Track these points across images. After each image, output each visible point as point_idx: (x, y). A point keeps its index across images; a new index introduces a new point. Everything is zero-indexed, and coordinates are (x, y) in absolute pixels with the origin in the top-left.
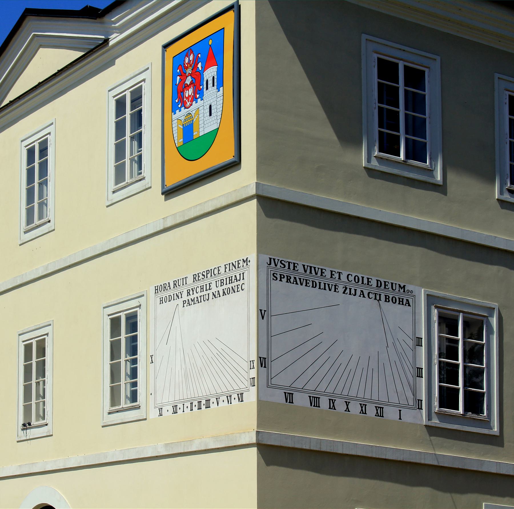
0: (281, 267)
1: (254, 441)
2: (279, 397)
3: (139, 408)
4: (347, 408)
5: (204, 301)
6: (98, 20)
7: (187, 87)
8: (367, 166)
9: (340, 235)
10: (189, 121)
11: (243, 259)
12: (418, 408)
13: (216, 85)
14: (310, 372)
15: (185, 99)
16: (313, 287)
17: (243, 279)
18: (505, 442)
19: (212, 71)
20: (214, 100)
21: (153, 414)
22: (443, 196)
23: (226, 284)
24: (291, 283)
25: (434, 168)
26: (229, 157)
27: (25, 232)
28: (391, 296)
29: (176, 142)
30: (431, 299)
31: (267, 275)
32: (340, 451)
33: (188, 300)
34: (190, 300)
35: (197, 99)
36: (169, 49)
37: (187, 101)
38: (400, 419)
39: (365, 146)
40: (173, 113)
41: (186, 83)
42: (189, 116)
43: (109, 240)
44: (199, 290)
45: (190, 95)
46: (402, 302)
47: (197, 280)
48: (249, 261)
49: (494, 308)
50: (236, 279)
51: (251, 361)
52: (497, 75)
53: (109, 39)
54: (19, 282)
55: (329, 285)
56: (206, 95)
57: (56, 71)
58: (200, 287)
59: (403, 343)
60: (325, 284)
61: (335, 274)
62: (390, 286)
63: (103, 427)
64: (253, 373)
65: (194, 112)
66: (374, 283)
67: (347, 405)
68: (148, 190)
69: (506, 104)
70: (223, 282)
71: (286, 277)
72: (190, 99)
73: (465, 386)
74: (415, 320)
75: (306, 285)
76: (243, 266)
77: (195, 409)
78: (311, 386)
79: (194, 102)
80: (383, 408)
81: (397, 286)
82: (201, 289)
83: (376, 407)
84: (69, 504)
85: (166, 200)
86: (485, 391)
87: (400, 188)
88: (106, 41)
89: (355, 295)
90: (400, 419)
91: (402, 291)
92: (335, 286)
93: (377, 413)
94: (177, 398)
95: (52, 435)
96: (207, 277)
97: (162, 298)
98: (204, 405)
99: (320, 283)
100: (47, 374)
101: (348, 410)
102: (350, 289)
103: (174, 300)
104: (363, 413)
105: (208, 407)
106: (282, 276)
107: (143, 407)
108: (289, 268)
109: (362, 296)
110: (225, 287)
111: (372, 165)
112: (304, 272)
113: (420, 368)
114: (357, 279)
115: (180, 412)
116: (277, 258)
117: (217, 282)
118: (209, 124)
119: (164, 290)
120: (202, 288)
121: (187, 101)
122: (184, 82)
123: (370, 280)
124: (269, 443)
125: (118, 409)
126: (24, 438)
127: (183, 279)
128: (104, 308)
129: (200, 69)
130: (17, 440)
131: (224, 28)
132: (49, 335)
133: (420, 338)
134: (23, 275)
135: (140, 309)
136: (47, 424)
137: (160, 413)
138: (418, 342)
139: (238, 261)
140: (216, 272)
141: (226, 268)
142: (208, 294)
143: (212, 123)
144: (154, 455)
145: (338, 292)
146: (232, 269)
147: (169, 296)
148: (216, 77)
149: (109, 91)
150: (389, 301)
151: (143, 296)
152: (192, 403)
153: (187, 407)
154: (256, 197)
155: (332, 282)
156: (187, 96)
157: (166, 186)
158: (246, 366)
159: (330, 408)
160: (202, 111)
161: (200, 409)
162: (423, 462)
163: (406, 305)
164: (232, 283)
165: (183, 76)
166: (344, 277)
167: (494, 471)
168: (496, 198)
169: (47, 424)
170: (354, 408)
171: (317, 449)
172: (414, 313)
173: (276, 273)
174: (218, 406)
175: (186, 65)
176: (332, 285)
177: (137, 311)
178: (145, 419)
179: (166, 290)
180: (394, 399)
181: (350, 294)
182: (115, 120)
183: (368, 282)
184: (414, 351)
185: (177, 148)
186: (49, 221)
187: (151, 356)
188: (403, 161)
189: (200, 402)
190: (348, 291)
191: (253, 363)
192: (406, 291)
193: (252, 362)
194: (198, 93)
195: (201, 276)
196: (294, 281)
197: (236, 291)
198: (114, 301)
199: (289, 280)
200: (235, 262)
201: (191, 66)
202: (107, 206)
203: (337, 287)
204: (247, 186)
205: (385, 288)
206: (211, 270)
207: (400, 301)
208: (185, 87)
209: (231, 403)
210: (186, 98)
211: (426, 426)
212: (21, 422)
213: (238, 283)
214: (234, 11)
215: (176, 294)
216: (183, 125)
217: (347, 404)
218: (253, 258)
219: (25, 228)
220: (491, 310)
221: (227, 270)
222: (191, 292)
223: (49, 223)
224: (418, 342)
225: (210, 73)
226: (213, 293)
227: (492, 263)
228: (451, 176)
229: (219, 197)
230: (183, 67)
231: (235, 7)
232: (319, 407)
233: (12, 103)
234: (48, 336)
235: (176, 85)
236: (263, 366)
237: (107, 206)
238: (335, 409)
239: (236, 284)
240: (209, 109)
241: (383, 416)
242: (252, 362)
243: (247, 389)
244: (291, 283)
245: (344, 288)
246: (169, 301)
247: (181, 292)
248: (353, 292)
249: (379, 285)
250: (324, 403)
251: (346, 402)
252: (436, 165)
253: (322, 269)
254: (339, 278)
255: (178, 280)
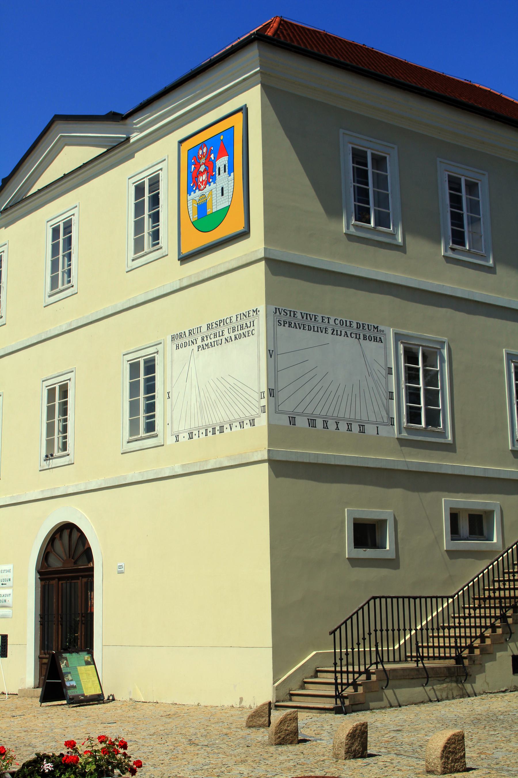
0: (284, 315)
1: (266, 457)
2: (284, 421)
3: (157, 436)
4: (337, 427)
5: (217, 345)
6: (121, 122)
7: (201, 173)
8: (347, 232)
9: (328, 288)
10: (203, 200)
11: (253, 310)
12: (391, 425)
13: (227, 171)
14: (308, 399)
15: (199, 183)
16: (308, 330)
17: (253, 326)
18: (457, 449)
19: (223, 160)
20: (226, 183)
21: (170, 440)
22: (403, 254)
23: (238, 330)
24: (292, 327)
25: (396, 233)
26: (240, 227)
27: (49, 296)
28: (368, 336)
29: (191, 218)
30: (398, 337)
31: (274, 321)
32: (333, 463)
33: (203, 345)
34: (204, 345)
35: (210, 182)
36: (184, 144)
37: (201, 185)
38: (378, 434)
39: (345, 217)
40: (188, 195)
41: (200, 170)
42: (203, 197)
43: (129, 300)
44: (212, 336)
45: (204, 179)
46: (376, 339)
47: (211, 328)
48: (259, 311)
49: (445, 342)
50: (247, 326)
51: (261, 392)
52: (439, 159)
53: (130, 137)
54: (43, 337)
55: (320, 328)
56: (219, 179)
57: (82, 164)
58: (213, 334)
59: (378, 373)
60: (318, 327)
61: (325, 319)
62: (366, 327)
63: (122, 454)
64: (264, 402)
65: (207, 193)
66: (354, 325)
67: (337, 425)
68: (165, 257)
69: (446, 181)
70: (235, 329)
71: (288, 323)
72: (204, 183)
73: (426, 404)
74: (386, 353)
75: (304, 329)
76: (253, 315)
77: (210, 434)
78: (309, 411)
79: (208, 186)
80: (364, 426)
81: (372, 327)
82: (214, 335)
83: (359, 425)
84: (89, 520)
85: (181, 265)
86: (440, 408)
87: (371, 249)
88: (128, 139)
89: (341, 335)
90: (378, 434)
91: (376, 330)
92: (326, 329)
93: (360, 430)
94: (193, 426)
95: (73, 463)
96: (220, 326)
97: (178, 344)
98: (218, 430)
99: (314, 327)
100: (69, 412)
101: (337, 428)
102: (337, 331)
103: (189, 345)
104: (349, 431)
105: (221, 432)
106: (285, 322)
107: (161, 435)
108: (290, 316)
109: (346, 336)
110: (236, 333)
111: (351, 231)
112: (301, 318)
113: (391, 392)
114: (342, 323)
115: (195, 437)
116: (281, 308)
117: (230, 330)
118: (221, 203)
119: (180, 338)
120: (215, 336)
121: (201, 185)
122: (199, 169)
123: (351, 323)
124: (278, 459)
125: (136, 438)
126: (47, 467)
127: (198, 328)
128: (124, 355)
129: (213, 159)
130: (40, 470)
131: (234, 126)
132: (71, 380)
133: (391, 368)
134: (47, 331)
135: (157, 354)
136: (69, 454)
137: (177, 440)
138: (389, 371)
139: (248, 312)
140: (228, 321)
141: (237, 318)
142: (221, 340)
143: (224, 201)
144: (172, 475)
145: (328, 333)
146: (243, 318)
147: (185, 343)
148: (227, 165)
149: (129, 179)
150: (366, 340)
151: (161, 343)
152: (207, 429)
153: (202, 433)
154: (264, 259)
155: (323, 326)
156: (201, 180)
157: (182, 253)
158: (256, 396)
159: (324, 428)
160: (215, 192)
161: (214, 434)
162: (396, 468)
163: (379, 342)
164: (243, 329)
165: (197, 165)
166: (332, 321)
167: (450, 472)
168: (442, 255)
169: (69, 454)
170: (343, 427)
171: (315, 462)
172: (386, 348)
173: (280, 320)
174: (231, 430)
175: (200, 156)
176: (323, 328)
177: (155, 357)
178: (163, 445)
179: (182, 337)
180: (373, 418)
181: (337, 335)
182: (135, 202)
183: (350, 324)
184: (386, 378)
185: (192, 222)
186: (72, 286)
187: (168, 393)
188: (373, 227)
189: (214, 429)
190: (335, 332)
191: (264, 394)
192: (379, 331)
193: (262, 393)
194: (211, 177)
195: (214, 325)
196: (294, 326)
197: (247, 335)
198: (133, 349)
199: (291, 325)
200: (246, 312)
201: (204, 157)
202: (127, 272)
203: (327, 329)
204: (256, 251)
205: (363, 329)
206: (224, 320)
207: (374, 339)
208: (199, 174)
209: (243, 428)
210: (200, 182)
211: (397, 438)
212: (44, 454)
213: (249, 329)
214: (242, 113)
215: (191, 340)
216: (198, 204)
217: (337, 423)
218: (262, 308)
219: (49, 293)
220: (442, 343)
221: (239, 319)
222: (205, 339)
223: (72, 288)
224: (389, 371)
225: (222, 162)
226: (225, 338)
227: (442, 307)
228: (408, 239)
229: (231, 260)
230: (197, 158)
231: (244, 109)
232: (316, 427)
233: (39, 191)
234: (70, 381)
235: (191, 172)
236: (272, 395)
237: (127, 272)
238: (328, 428)
239: (247, 330)
240: (221, 191)
241: (364, 433)
242: (262, 393)
243: (258, 415)
244: (292, 327)
245: (333, 330)
246: (185, 347)
247: (195, 339)
248: (339, 333)
249: (359, 327)
250: (319, 424)
251: (336, 422)
252: (397, 230)
253: (315, 316)
254: (329, 322)
255: (193, 329)
